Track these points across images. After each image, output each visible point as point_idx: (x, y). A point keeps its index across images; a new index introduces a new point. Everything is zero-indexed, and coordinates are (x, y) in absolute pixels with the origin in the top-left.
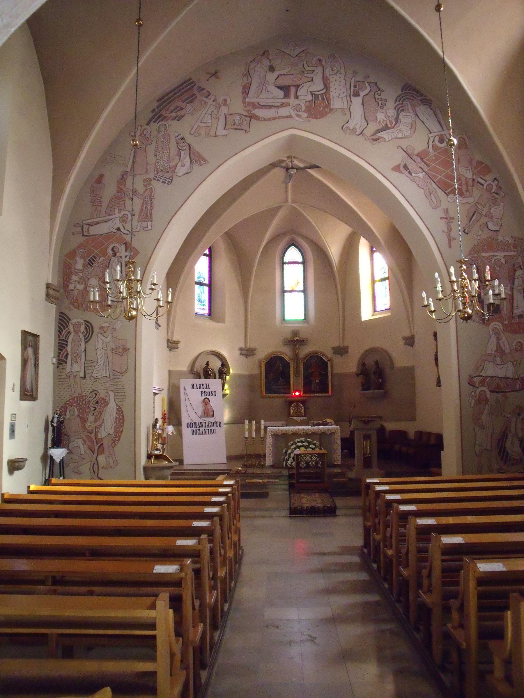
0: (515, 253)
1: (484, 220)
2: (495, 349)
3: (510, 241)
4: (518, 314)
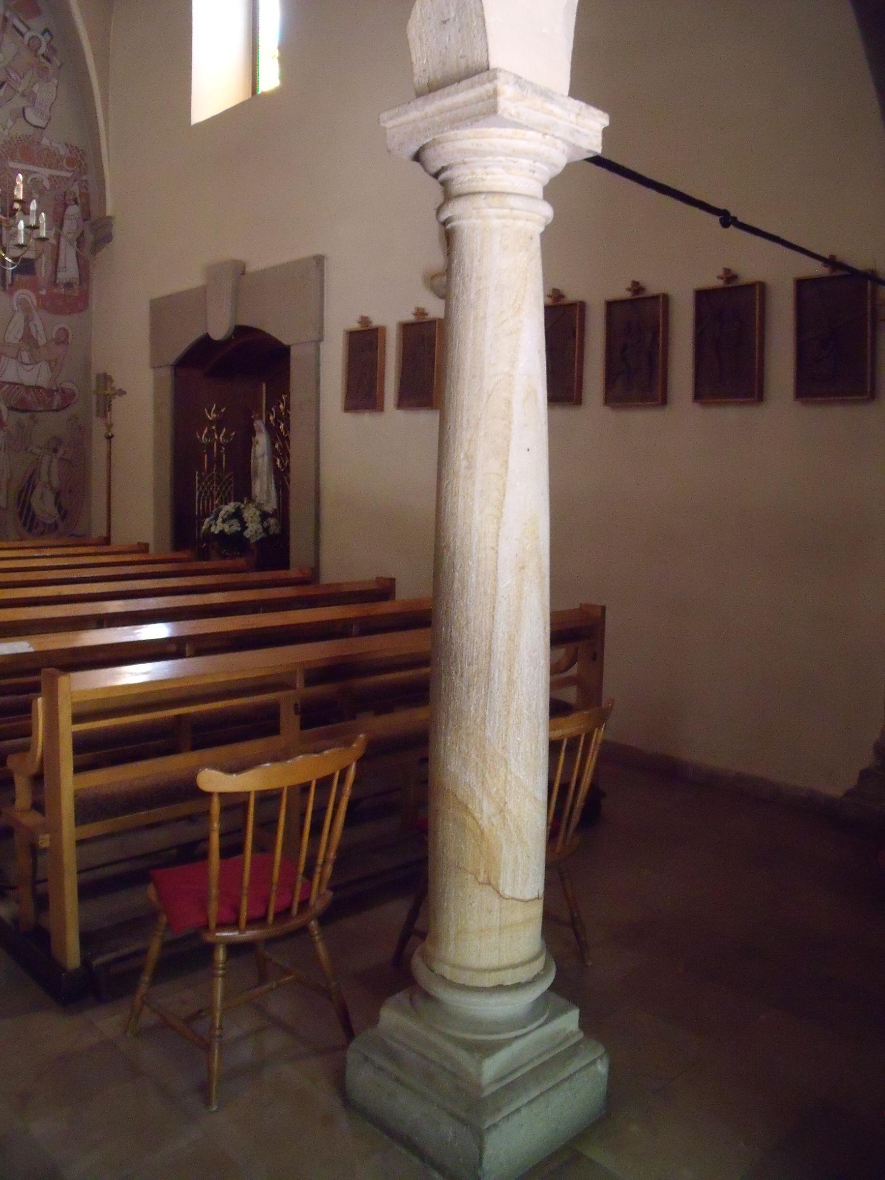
0: (68, 175)
1: (18, 102)
2: (20, 336)
3: (62, 152)
4: (65, 281)
